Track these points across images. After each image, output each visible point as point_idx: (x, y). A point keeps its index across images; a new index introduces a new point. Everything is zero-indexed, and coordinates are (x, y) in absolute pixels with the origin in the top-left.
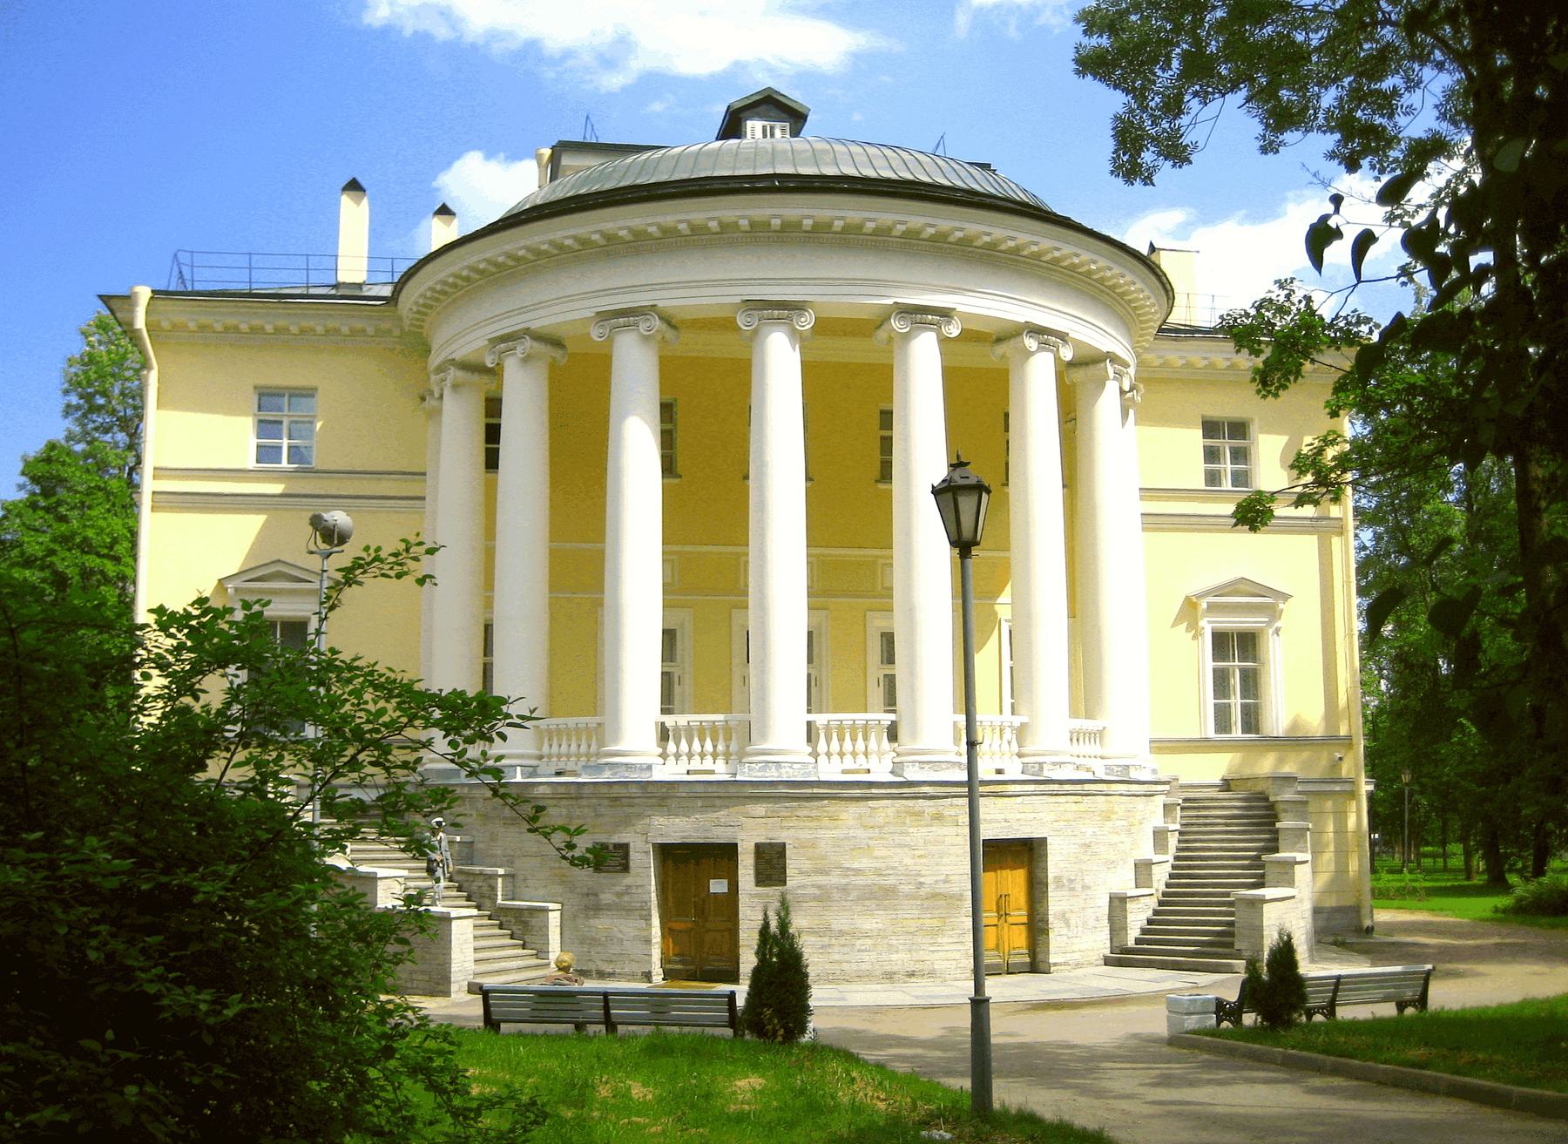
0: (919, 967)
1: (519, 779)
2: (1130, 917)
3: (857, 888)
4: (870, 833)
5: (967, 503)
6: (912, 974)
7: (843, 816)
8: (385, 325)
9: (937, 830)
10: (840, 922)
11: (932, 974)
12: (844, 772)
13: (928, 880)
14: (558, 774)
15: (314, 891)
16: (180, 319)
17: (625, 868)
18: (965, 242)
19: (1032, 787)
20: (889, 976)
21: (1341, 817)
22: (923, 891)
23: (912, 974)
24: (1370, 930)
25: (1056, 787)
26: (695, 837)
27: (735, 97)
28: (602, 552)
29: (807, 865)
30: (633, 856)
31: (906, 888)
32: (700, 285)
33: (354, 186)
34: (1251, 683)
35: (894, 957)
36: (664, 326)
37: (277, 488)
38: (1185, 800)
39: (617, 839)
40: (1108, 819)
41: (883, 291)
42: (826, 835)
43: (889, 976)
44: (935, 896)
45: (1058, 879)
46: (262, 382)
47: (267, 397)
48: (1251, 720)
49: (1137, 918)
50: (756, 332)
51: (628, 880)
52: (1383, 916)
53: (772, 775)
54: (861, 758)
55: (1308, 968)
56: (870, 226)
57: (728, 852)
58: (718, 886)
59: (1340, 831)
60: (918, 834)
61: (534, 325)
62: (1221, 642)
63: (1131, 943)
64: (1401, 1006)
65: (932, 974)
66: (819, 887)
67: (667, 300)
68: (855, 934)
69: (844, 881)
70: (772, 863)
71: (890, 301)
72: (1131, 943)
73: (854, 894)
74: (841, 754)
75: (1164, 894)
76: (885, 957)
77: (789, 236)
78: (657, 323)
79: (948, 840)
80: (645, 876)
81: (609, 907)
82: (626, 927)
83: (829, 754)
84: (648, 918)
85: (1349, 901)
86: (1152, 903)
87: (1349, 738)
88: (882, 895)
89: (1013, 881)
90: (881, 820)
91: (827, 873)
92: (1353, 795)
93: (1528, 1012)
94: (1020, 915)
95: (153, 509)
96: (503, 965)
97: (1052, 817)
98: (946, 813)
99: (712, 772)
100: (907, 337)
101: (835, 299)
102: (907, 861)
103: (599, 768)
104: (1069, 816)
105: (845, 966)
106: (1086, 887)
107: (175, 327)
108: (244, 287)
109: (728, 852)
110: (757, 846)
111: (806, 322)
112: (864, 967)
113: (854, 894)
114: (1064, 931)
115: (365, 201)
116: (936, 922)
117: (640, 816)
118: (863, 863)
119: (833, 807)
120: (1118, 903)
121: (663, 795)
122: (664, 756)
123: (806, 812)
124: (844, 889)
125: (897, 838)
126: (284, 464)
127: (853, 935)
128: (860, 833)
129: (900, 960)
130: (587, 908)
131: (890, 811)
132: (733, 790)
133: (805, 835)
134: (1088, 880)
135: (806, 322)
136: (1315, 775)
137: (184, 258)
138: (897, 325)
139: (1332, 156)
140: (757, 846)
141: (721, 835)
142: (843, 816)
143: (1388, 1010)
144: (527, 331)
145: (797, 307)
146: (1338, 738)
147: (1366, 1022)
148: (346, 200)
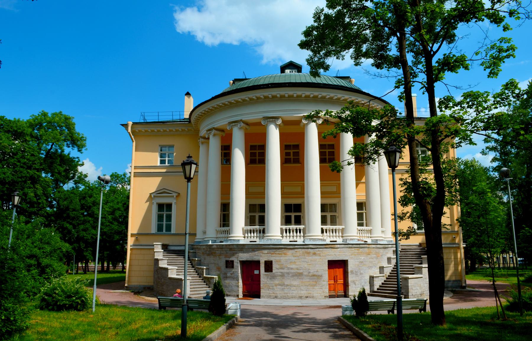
0: (309, 295)
1: (210, 243)
2: (375, 282)
3: (292, 273)
4: (295, 258)
5: (187, 168)
6: (307, 297)
7: (288, 253)
8: (190, 128)
9: (315, 257)
10: (287, 282)
11: (313, 297)
12: (331, 241)
13: (311, 271)
14: (221, 242)
15: (60, 273)
16: (140, 129)
17: (233, 267)
18: (331, 98)
19: (343, 246)
20: (301, 297)
21: (456, 254)
22: (310, 274)
23: (307, 297)
24: (464, 287)
25: (351, 246)
26: (249, 259)
27: (281, 64)
28: (230, 184)
29: (278, 267)
30: (235, 264)
31: (305, 273)
32: (252, 114)
33: (188, 94)
34: (169, 218)
35: (302, 292)
36: (245, 125)
37: (164, 170)
38: (402, 249)
39: (231, 259)
40: (369, 254)
41: (301, 112)
42: (283, 259)
43: (301, 297)
44: (314, 275)
45: (352, 272)
46: (160, 144)
47: (162, 148)
48: (169, 228)
49: (377, 284)
50: (267, 125)
51: (233, 270)
52: (469, 282)
53: (269, 243)
54: (295, 238)
55: (370, 299)
56: (320, 96)
57: (258, 262)
58: (256, 272)
59: (456, 258)
60: (309, 258)
61: (215, 126)
62: (161, 207)
63: (375, 290)
64: (389, 312)
65: (313, 297)
66: (281, 273)
67: (245, 118)
68: (291, 286)
69: (288, 271)
70: (269, 266)
71: (302, 115)
72: (375, 290)
73: (291, 275)
74: (290, 237)
75: (389, 276)
76: (299, 292)
77: (274, 99)
78: (242, 124)
79: (318, 260)
80: (238, 270)
81: (229, 277)
82: (233, 282)
83: (286, 237)
84: (238, 280)
85: (458, 278)
86: (385, 279)
87: (458, 231)
88: (299, 275)
89: (339, 272)
90: (298, 255)
91: (283, 269)
92: (459, 248)
93: (460, 315)
94: (341, 281)
95: (134, 176)
96: (201, 292)
97: (350, 254)
98: (317, 253)
99: (336, 241)
100: (307, 124)
101: (291, 115)
102: (306, 266)
103: (227, 241)
104: (355, 254)
105: (288, 294)
106: (361, 274)
107: (139, 131)
108: (157, 121)
109: (258, 262)
110: (265, 261)
111: (279, 122)
112: (294, 295)
113: (291, 275)
114: (354, 286)
115: (191, 98)
116: (314, 283)
117: (236, 253)
118: (293, 266)
119: (285, 251)
120: (372, 278)
121: (242, 248)
122: (282, 237)
123: (278, 252)
124: (288, 273)
125: (303, 260)
126: (167, 164)
127: (291, 286)
128: (293, 258)
129: (304, 293)
130: (224, 277)
131: (301, 252)
132: (366, 246)
133: (278, 258)
134: (362, 271)
135: (279, 122)
136: (448, 242)
137: (143, 114)
138: (304, 121)
139: (373, 65)
140: (265, 261)
141: (256, 258)
142: (288, 253)
143: (417, 311)
144: (214, 128)
145: (277, 118)
146: (455, 231)
147: (378, 315)
148: (186, 97)
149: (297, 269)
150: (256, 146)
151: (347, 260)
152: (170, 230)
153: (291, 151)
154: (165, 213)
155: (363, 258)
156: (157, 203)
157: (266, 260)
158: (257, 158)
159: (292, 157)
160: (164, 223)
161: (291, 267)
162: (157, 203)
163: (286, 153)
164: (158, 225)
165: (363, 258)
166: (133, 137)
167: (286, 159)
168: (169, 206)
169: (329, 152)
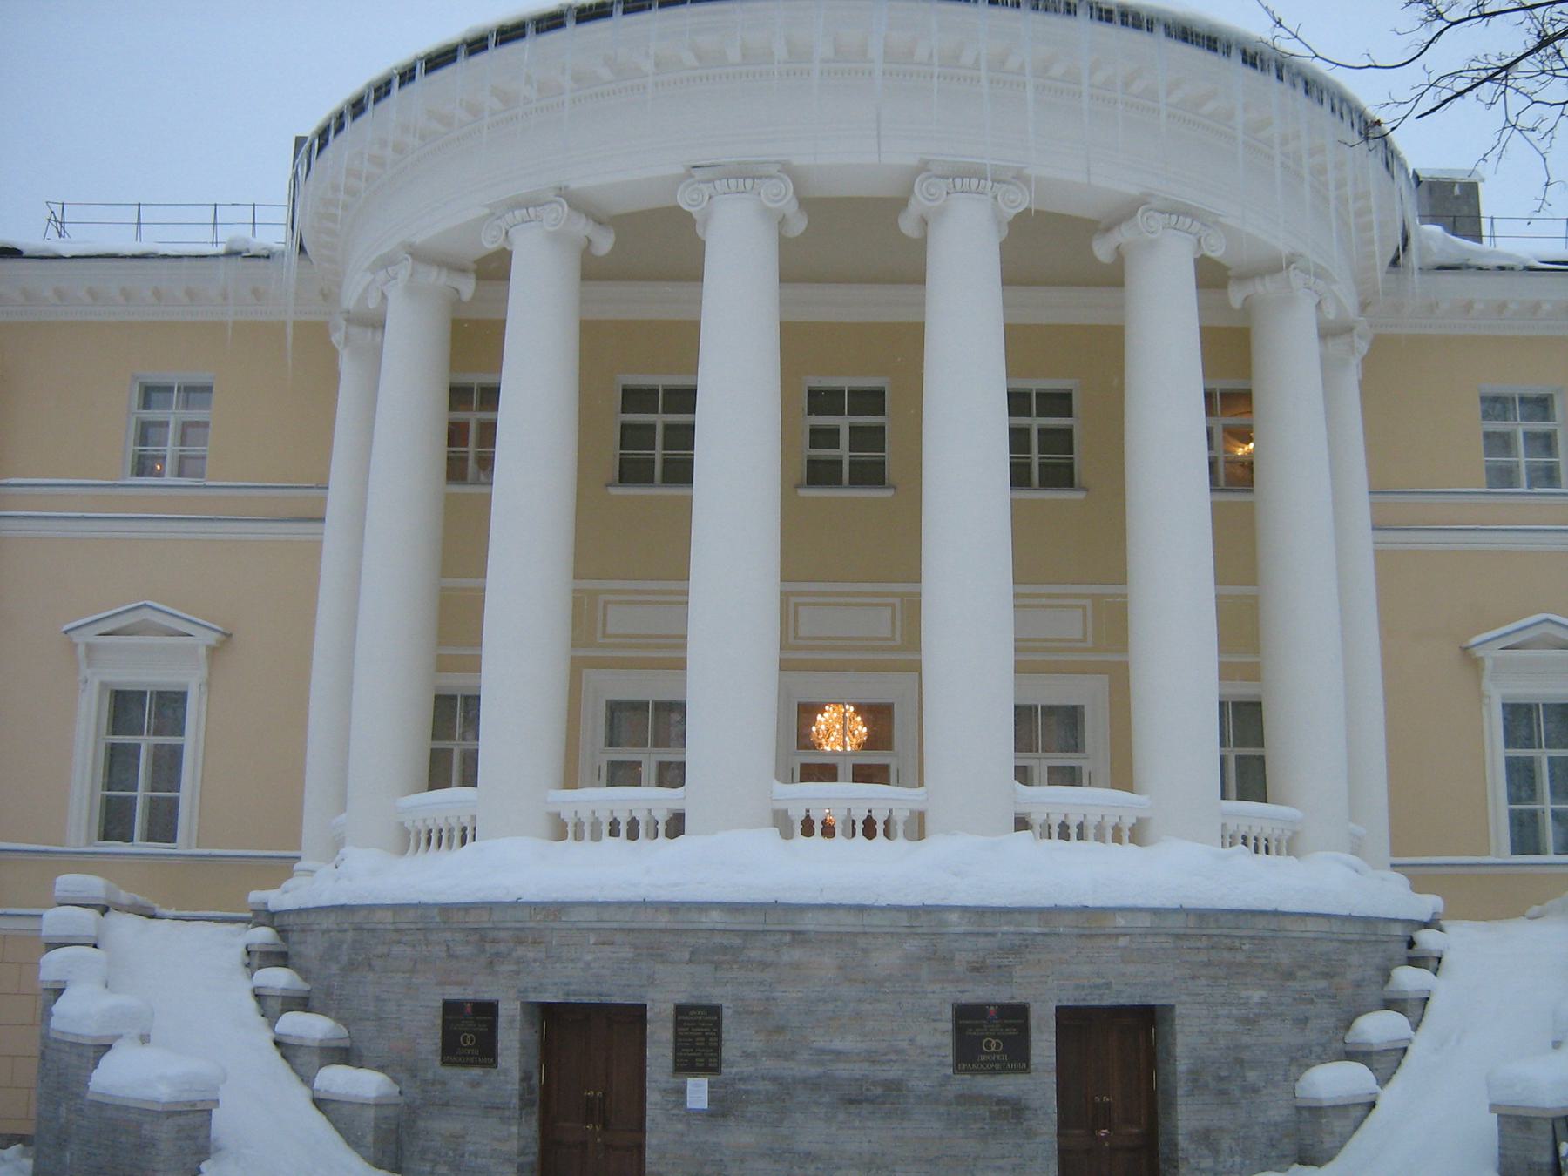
34: (168, 765)
48: (163, 826)
110: (680, 1010)
118: (848, 1043)
124: (814, 1084)
134: (1252, 1076)
140: (680, 1010)
149: (871, 1058)
150: (654, 391)
151: (1173, 1007)
152: (170, 836)
153: (843, 422)
154: (146, 742)
155: (1257, 995)
156: (103, 685)
157: (683, 999)
158: (658, 453)
159: (844, 452)
160: (141, 794)
161: (837, 1044)
162: (103, 685)
163: (815, 431)
164: (108, 802)
165: (1257, 995)
166: (898, 623)
167: (812, 463)
168: (171, 704)
169: (1043, 431)
